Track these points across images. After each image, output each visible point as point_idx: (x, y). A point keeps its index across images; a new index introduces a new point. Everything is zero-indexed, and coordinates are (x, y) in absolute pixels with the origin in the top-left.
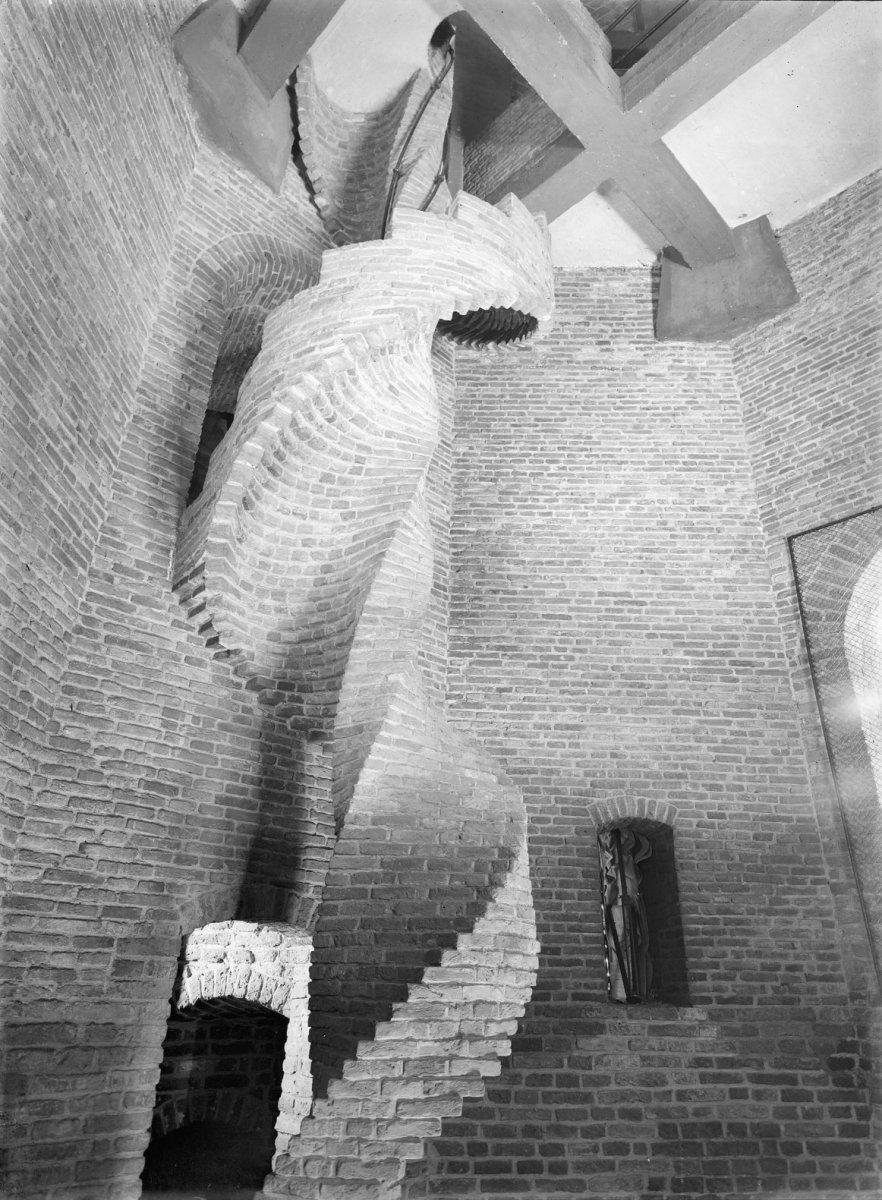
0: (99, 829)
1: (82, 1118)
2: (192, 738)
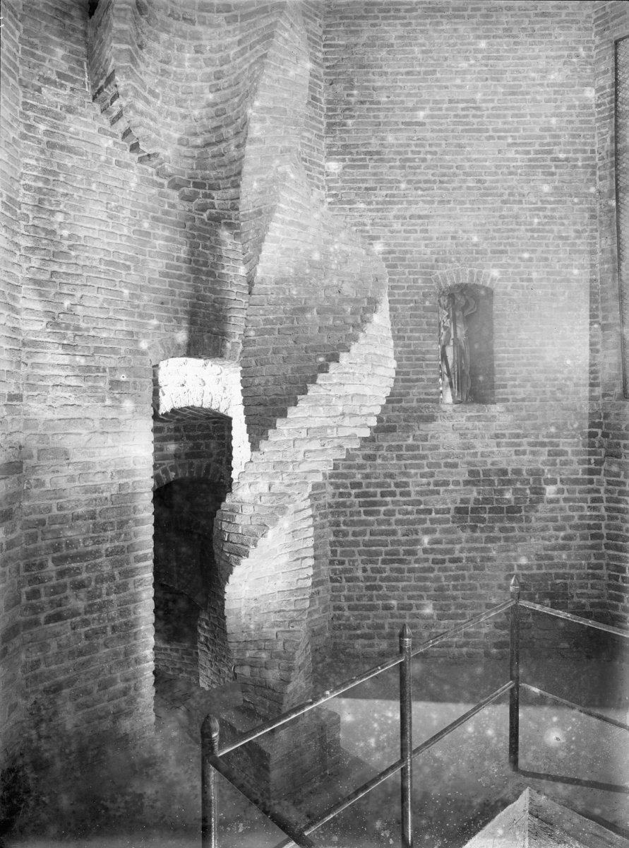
0: (79, 294)
1: (109, 471)
2: (133, 228)
